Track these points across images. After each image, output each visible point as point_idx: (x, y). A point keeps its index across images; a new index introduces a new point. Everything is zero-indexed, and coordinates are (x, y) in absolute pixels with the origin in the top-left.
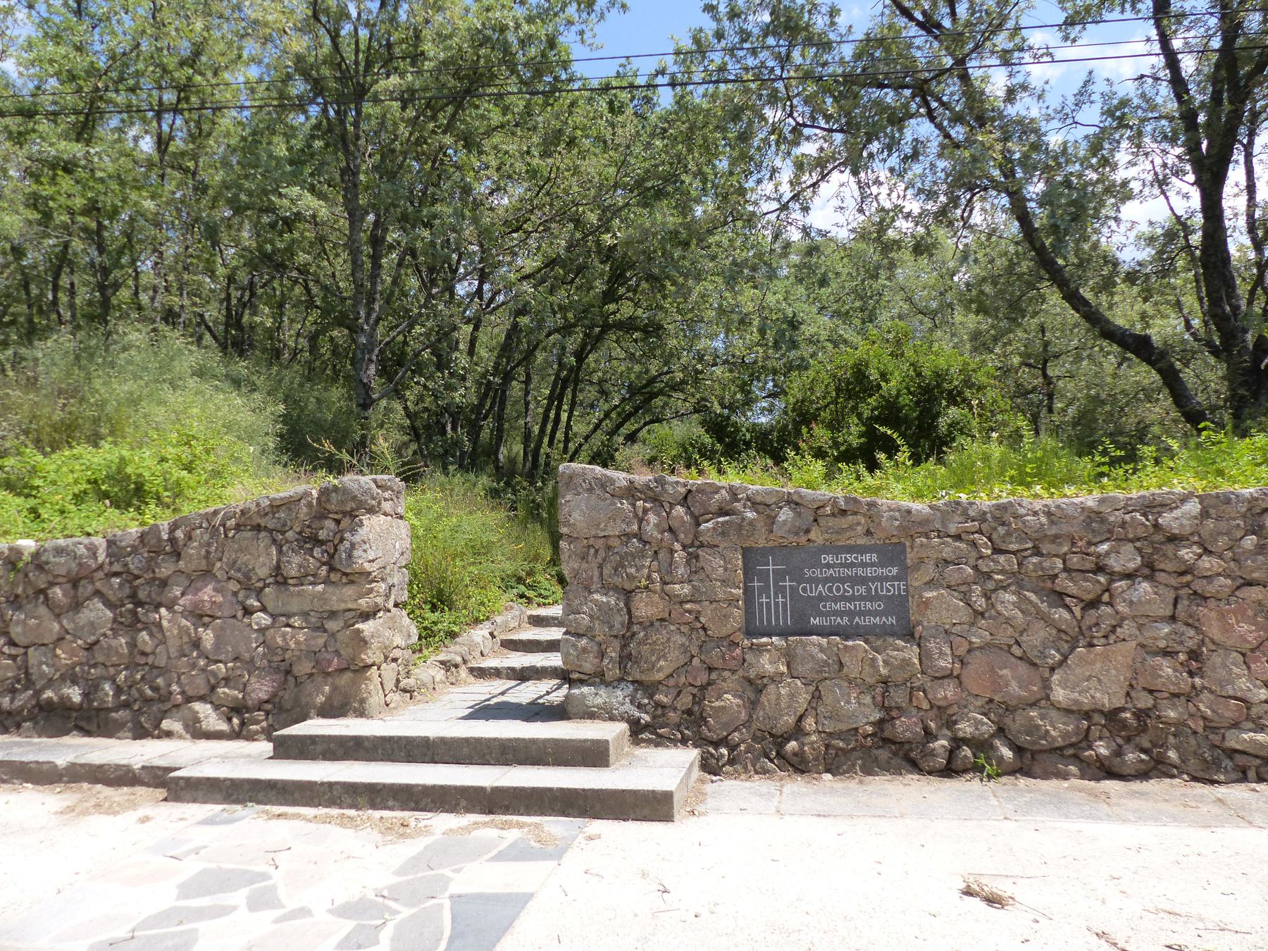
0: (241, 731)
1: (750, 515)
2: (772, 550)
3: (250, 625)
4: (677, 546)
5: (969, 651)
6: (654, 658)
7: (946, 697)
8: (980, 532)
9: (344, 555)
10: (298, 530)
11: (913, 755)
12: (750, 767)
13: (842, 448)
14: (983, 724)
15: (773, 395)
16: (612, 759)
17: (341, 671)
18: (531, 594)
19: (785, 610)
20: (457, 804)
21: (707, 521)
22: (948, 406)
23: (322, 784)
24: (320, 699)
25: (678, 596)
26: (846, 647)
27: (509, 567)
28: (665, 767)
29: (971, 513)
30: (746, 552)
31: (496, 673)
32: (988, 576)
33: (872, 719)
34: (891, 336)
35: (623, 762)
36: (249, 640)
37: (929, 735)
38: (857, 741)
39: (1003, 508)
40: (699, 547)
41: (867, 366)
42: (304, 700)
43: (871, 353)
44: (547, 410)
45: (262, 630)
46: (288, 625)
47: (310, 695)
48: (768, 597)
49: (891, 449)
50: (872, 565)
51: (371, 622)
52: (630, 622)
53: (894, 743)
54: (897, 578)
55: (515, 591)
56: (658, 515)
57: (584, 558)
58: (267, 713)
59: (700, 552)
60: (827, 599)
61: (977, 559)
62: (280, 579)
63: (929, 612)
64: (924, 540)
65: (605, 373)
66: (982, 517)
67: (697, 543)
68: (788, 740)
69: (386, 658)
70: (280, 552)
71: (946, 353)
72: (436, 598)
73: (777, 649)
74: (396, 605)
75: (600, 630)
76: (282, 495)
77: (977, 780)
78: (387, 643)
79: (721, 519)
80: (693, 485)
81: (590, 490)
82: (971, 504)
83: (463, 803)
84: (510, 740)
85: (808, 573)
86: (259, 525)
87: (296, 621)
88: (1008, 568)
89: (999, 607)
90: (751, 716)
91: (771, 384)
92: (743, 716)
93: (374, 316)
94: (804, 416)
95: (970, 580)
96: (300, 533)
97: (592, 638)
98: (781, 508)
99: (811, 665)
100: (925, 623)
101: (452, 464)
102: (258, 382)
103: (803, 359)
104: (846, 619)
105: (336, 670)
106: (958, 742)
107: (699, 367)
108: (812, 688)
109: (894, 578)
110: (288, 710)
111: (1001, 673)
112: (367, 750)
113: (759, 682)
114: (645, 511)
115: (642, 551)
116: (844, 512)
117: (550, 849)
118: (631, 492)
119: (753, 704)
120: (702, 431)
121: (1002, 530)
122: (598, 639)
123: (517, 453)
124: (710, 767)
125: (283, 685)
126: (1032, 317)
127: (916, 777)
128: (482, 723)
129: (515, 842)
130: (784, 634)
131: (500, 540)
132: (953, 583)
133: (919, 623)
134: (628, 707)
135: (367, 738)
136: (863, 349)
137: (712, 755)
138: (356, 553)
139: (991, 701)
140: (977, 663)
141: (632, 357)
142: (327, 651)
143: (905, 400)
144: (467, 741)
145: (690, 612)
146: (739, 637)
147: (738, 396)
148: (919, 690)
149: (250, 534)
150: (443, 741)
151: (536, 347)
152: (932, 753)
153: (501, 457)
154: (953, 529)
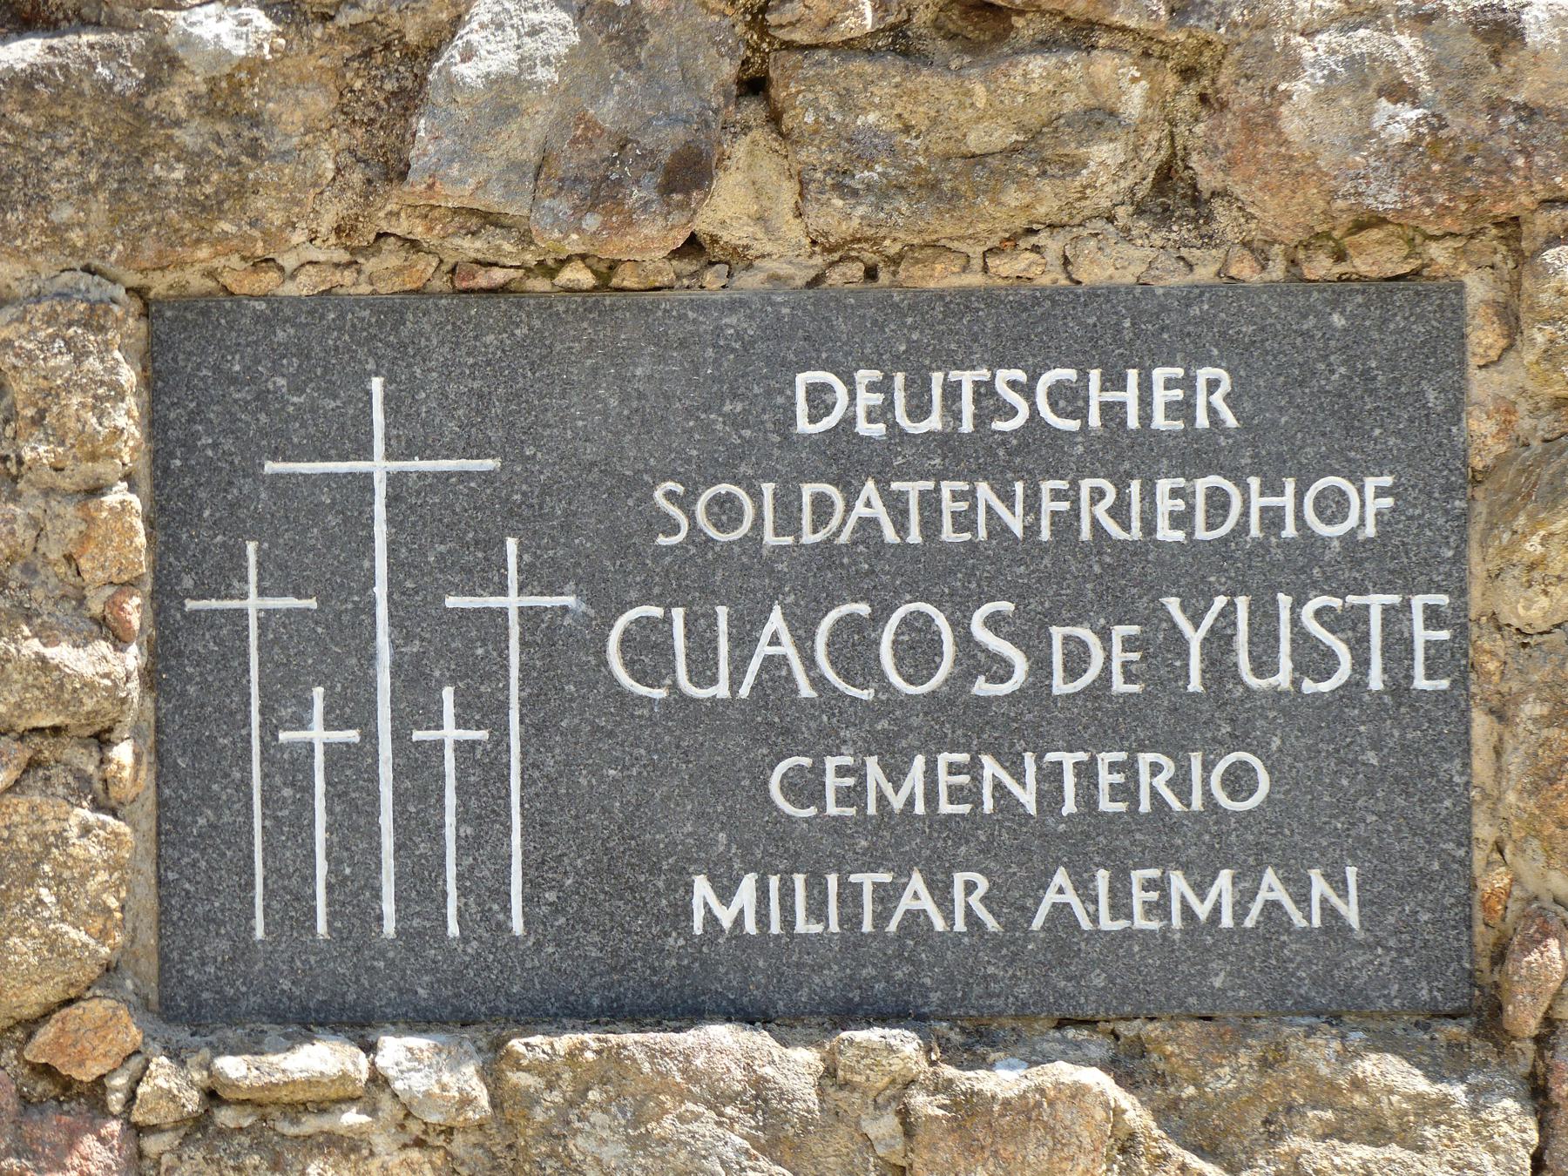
19: (484, 817)
26: (968, 1107)
30: (180, 340)
48: (351, 708)
50: (1196, 453)
54: (1381, 561)
60: (829, 723)
85: (681, 516)
104: (971, 889)
109: (1362, 563)
130: (470, 1011)
146: (102, 1037)
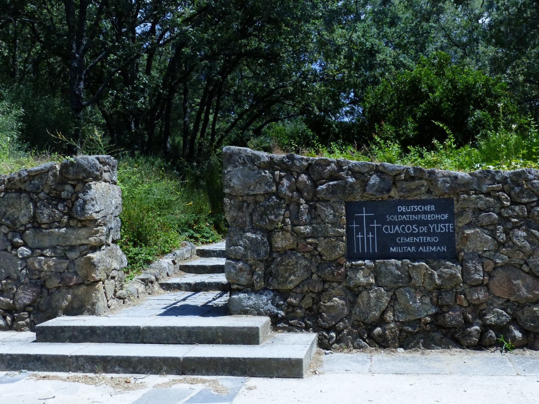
0: (12, 325)
1: (351, 180)
2: (364, 204)
3: (16, 255)
4: (302, 201)
5: (494, 269)
6: (287, 275)
7: (479, 298)
8: (503, 190)
9: (79, 208)
10: (47, 191)
11: (457, 335)
12: (350, 344)
13: (402, 138)
14: (503, 315)
15: (353, 102)
16: (261, 339)
17: (79, 285)
18: (198, 235)
20: (161, 369)
21: (322, 184)
22: (474, 110)
23: (71, 357)
24: (65, 303)
25: (303, 233)
26: (414, 266)
27: (183, 217)
28: (296, 344)
29: (497, 178)
30: (348, 205)
31: (178, 287)
32: (508, 219)
33: (430, 313)
34: (436, 61)
35: (268, 341)
36: (16, 265)
37: (468, 323)
38: (420, 327)
39: (519, 175)
40: (316, 202)
41: (420, 82)
42: (54, 304)
43: (423, 73)
44: (199, 113)
45: (25, 259)
46: (42, 255)
47: (58, 301)
48: (362, 234)
49: (442, 137)
50: (431, 212)
51: (98, 253)
52: (271, 252)
53: (444, 328)
55: (187, 234)
56: (289, 180)
57: (240, 209)
58: (30, 313)
59: (318, 205)
60: (401, 235)
61: (501, 208)
62: (35, 224)
63: (468, 243)
64: (466, 196)
65: (239, 87)
66: (504, 180)
67: (316, 199)
68: (375, 327)
69: (108, 276)
70: (35, 207)
71: (473, 72)
72: (138, 237)
73: (368, 267)
74: (114, 242)
75: (251, 258)
76: (36, 168)
77: (498, 351)
78: (109, 266)
79: (331, 183)
80: (312, 160)
81: (244, 164)
82: (497, 172)
83: (165, 368)
84: (193, 328)
85: (389, 218)
86: (20, 189)
87: (48, 253)
88: (521, 214)
89: (515, 240)
90: (351, 312)
91: (352, 94)
92: (346, 311)
93: (83, 47)
94: (375, 116)
95: (496, 222)
96: (48, 194)
97: (246, 262)
98: (371, 175)
99: (390, 278)
100: (466, 251)
101: (137, 149)
102: (4, 94)
103: (375, 77)
104: (413, 248)
105: (75, 285)
106: (486, 327)
107: (304, 83)
108: (391, 293)
109: (445, 221)
110: (44, 311)
111: (515, 282)
112: (99, 336)
113: (356, 289)
114: (281, 178)
115: (279, 204)
116: (413, 178)
117: (224, 395)
118: (271, 165)
119: (352, 304)
120: (304, 126)
121: (517, 189)
122: (250, 262)
123: (179, 142)
124: (324, 344)
125: (40, 295)
126: (533, 48)
127: (459, 350)
128: (173, 317)
129: (201, 391)
130: (372, 258)
131: (177, 200)
132: (484, 224)
133: (462, 250)
134: (270, 306)
135: (99, 328)
136: (416, 69)
137: (325, 337)
138: (87, 207)
139: (508, 301)
140: (500, 275)
141: (257, 76)
142: (69, 272)
143: (446, 105)
144: (164, 329)
145: (311, 244)
146: (343, 260)
147: (331, 103)
148: (461, 293)
149: (14, 195)
150: (149, 329)
151: (191, 70)
152: (470, 335)
153: (168, 145)
154: (485, 188)
